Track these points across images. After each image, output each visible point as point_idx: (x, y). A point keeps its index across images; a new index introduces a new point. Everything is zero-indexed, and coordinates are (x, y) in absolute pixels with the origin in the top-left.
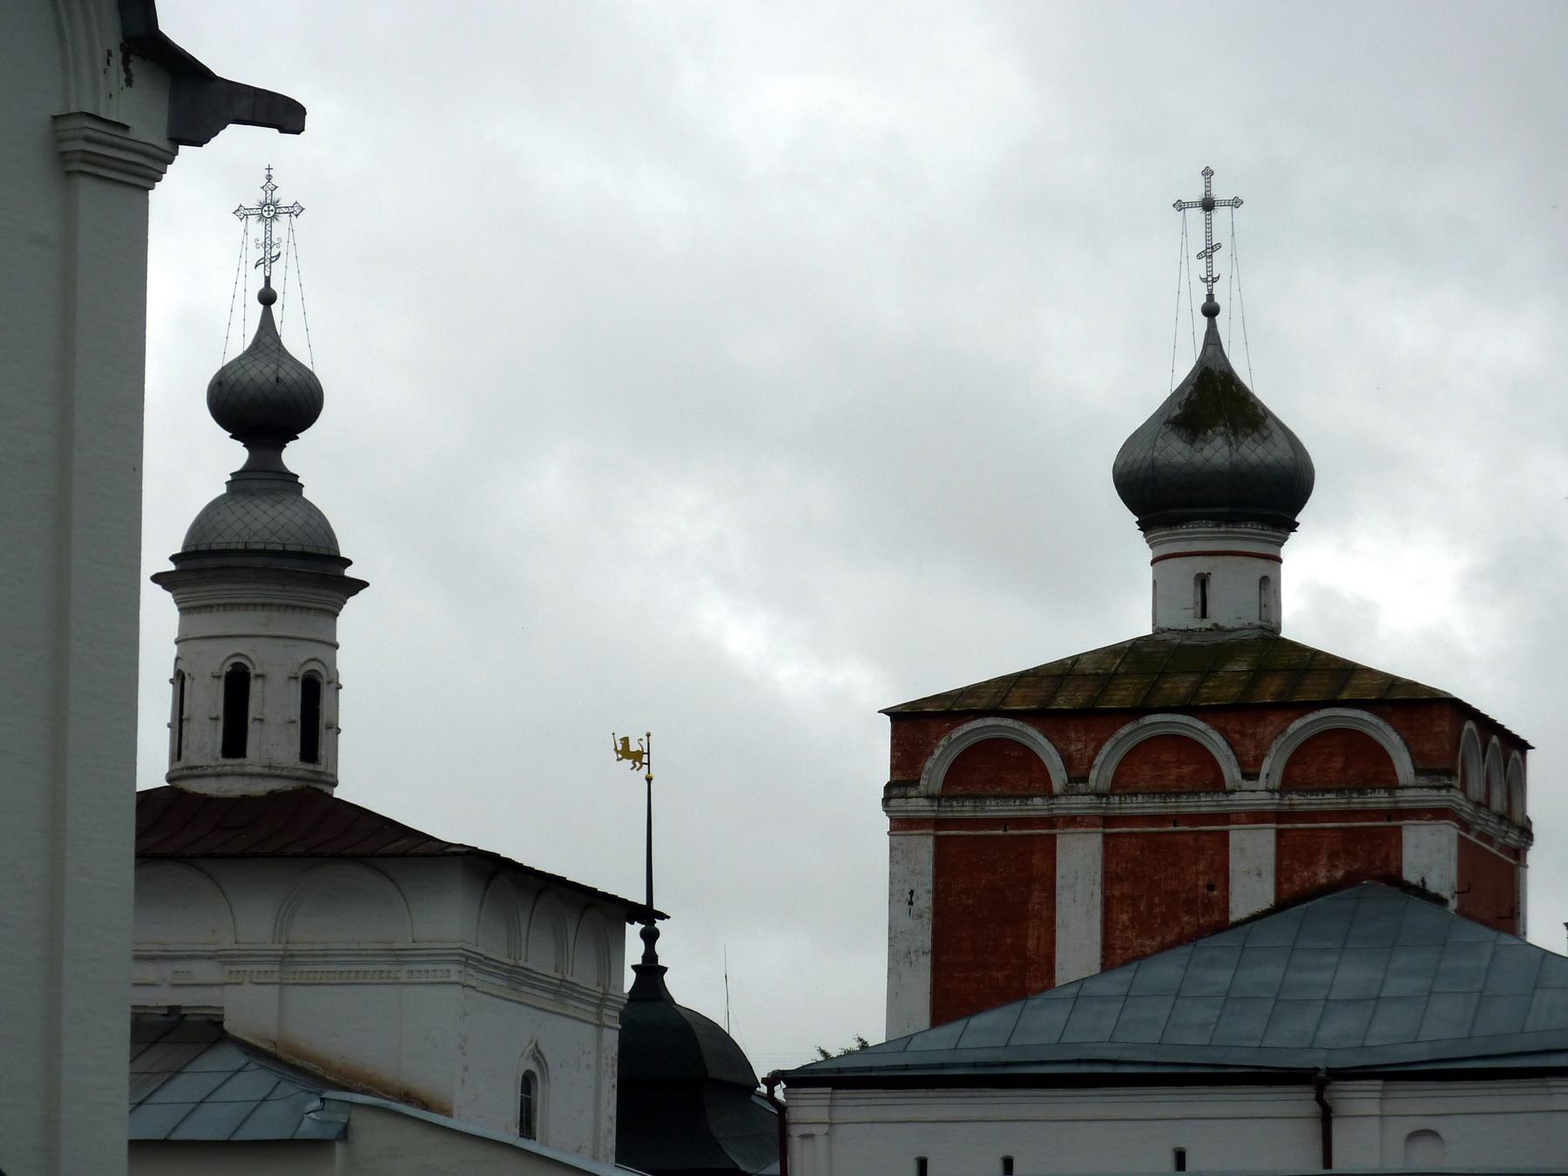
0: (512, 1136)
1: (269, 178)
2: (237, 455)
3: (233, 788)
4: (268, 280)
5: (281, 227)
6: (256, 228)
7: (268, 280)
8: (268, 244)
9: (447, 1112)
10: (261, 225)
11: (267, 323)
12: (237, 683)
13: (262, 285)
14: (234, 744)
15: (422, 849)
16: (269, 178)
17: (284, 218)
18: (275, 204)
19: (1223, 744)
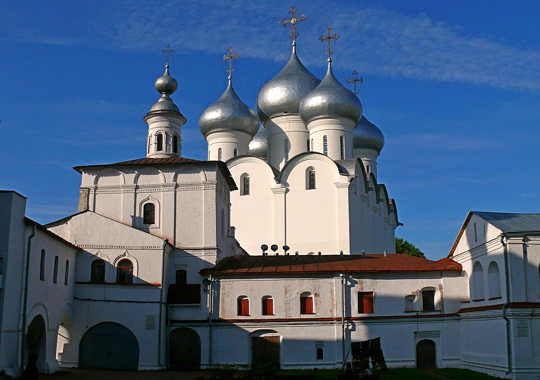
3: (159, 157)
14: (159, 148)
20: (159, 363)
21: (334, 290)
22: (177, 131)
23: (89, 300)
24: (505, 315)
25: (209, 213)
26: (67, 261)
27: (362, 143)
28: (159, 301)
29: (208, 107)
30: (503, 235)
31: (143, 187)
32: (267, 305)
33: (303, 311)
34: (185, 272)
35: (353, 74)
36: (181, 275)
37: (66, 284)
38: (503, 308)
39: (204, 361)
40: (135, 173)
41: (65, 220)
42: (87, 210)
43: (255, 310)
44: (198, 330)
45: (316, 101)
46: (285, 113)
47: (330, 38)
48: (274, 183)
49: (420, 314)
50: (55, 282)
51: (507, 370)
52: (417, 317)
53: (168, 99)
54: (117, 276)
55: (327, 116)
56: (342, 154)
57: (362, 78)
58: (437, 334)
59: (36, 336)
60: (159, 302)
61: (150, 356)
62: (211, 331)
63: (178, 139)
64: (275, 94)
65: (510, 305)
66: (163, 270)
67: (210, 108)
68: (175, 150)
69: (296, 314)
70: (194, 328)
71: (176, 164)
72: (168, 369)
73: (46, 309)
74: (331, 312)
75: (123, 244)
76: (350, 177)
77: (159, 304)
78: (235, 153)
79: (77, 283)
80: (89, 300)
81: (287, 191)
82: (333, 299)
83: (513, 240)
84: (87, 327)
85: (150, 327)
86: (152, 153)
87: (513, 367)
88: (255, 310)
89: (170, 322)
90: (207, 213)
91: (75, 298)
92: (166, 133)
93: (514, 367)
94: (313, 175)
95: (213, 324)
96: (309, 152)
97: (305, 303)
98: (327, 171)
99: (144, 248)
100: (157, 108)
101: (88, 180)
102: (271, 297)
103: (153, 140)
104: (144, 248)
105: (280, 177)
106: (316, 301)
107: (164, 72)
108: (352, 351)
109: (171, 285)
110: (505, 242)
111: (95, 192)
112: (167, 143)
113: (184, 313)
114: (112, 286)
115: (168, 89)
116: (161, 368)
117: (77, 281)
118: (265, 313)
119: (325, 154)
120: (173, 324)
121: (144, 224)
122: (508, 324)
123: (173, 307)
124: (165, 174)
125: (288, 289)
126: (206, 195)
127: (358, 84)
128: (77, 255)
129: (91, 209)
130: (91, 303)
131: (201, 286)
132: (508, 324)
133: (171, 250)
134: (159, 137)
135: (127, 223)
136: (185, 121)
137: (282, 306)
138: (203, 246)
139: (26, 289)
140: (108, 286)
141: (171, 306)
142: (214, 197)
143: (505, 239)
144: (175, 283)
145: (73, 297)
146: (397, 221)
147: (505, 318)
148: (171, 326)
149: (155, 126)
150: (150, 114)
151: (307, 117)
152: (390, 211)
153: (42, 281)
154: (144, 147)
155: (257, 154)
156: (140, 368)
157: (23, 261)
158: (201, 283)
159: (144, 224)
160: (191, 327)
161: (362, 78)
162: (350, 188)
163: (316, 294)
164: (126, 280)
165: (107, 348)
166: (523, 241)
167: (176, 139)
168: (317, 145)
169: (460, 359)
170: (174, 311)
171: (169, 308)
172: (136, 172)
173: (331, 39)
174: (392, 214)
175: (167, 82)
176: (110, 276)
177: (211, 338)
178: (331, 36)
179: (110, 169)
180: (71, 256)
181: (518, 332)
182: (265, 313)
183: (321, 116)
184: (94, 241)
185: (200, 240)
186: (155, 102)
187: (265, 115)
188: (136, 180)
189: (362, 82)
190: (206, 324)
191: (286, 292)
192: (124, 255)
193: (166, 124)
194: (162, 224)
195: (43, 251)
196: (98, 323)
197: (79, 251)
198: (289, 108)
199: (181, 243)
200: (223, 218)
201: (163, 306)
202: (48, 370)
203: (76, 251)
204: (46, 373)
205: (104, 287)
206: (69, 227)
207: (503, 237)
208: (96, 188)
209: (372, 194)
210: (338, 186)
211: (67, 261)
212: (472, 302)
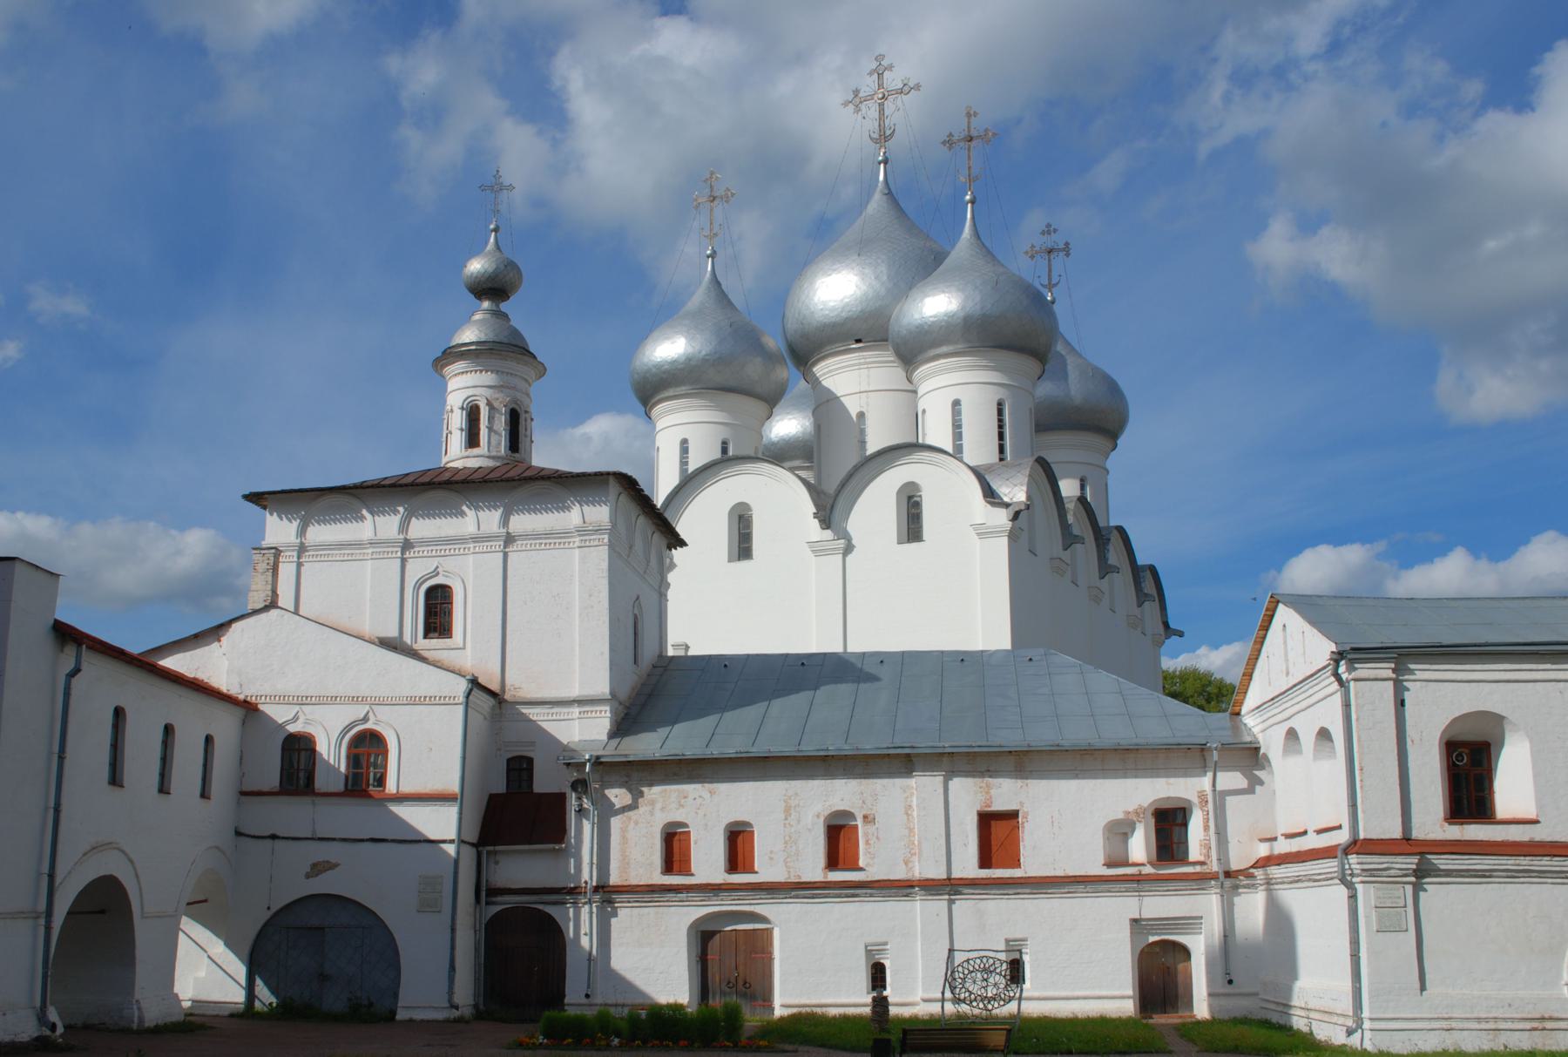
3: (473, 463)
14: (472, 440)
20: (450, 1000)
21: (914, 804)
22: (519, 395)
23: (274, 837)
24: (1344, 875)
26: (209, 740)
27: (1063, 420)
29: (651, 331)
30: (1338, 657)
32: (738, 843)
33: (833, 862)
34: (530, 761)
35: (1043, 233)
36: (520, 768)
37: (204, 795)
38: (1339, 854)
40: (396, 512)
41: (216, 632)
42: (272, 605)
43: (708, 862)
45: (937, 304)
46: (858, 341)
47: (971, 139)
48: (814, 530)
49: (1148, 870)
50: (163, 789)
51: (1350, 1023)
52: (1138, 879)
53: (499, 315)
55: (960, 347)
56: (1002, 449)
57: (1067, 244)
58: (1189, 923)
59: (101, 924)
61: (436, 972)
64: (836, 289)
65: (1358, 846)
66: (464, 758)
67: (656, 334)
68: (514, 442)
69: (813, 867)
71: (515, 481)
73: (131, 861)
74: (906, 864)
75: (364, 690)
76: (1011, 511)
78: (724, 450)
79: (244, 793)
80: (274, 837)
81: (849, 549)
82: (911, 830)
83: (1364, 670)
85: (427, 905)
86: (456, 455)
87: (1366, 1014)
88: (708, 862)
89: (485, 892)
91: (238, 833)
92: (489, 404)
94: (918, 505)
96: (914, 447)
97: (839, 838)
98: (951, 494)
99: (414, 701)
100: (469, 335)
101: (279, 529)
102: (686, 825)
103: (457, 420)
104: (414, 701)
105: (830, 508)
106: (866, 834)
107: (487, 243)
110: (1344, 677)
112: (490, 429)
113: (520, 869)
114: (333, 800)
115: (493, 289)
116: (456, 1014)
117: (246, 788)
118: (668, 868)
119: (957, 453)
121: (426, 637)
122: (1353, 897)
123: (496, 853)
124: (585, 508)
125: (793, 803)
127: (1058, 261)
129: (285, 599)
130: (279, 844)
132: (1353, 897)
133: (491, 703)
134: (473, 414)
136: (542, 370)
138: (575, 692)
139: (57, 810)
141: (488, 853)
142: (605, 565)
143: (1342, 669)
146: (1166, 625)
147: (1343, 881)
148: (487, 903)
149: (464, 385)
150: (451, 354)
151: (912, 351)
152: (1142, 597)
154: (435, 435)
155: (780, 455)
156: (401, 1015)
159: (426, 637)
160: (540, 907)
161: (1067, 244)
162: (1013, 536)
163: (865, 817)
165: (318, 956)
166: (1394, 671)
167: (515, 418)
168: (937, 432)
169: (1256, 994)
170: (497, 863)
172: (401, 509)
173: (973, 144)
174: (1151, 608)
175: (491, 270)
178: (974, 133)
180: (225, 726)
181: (1380, 920)
182: (1109, 865)
183: (944, 349)
184: (289, 684)
185: (568, 682)
186: (466, 320)
187: (807, 349)
188: (404, 527)
189: (1068, 255)
191: (787, 811)
192: (365, 719)
193: (488, 378)
194: (472, 644)
195: (119, 713)
197: (248, 709)
198: (863, 331)
199: (522, 683)
200: (1536, 653)
202: (141, 1019)
203: (239, 713)
204: (135, 1026)
205: (314, 804)
206: (223, 650)
207: (1337, 662)
208: (302, 549)
209: (1086, 552)
210: (983, 532)
211: (209, 740)
212: (1281, 839)
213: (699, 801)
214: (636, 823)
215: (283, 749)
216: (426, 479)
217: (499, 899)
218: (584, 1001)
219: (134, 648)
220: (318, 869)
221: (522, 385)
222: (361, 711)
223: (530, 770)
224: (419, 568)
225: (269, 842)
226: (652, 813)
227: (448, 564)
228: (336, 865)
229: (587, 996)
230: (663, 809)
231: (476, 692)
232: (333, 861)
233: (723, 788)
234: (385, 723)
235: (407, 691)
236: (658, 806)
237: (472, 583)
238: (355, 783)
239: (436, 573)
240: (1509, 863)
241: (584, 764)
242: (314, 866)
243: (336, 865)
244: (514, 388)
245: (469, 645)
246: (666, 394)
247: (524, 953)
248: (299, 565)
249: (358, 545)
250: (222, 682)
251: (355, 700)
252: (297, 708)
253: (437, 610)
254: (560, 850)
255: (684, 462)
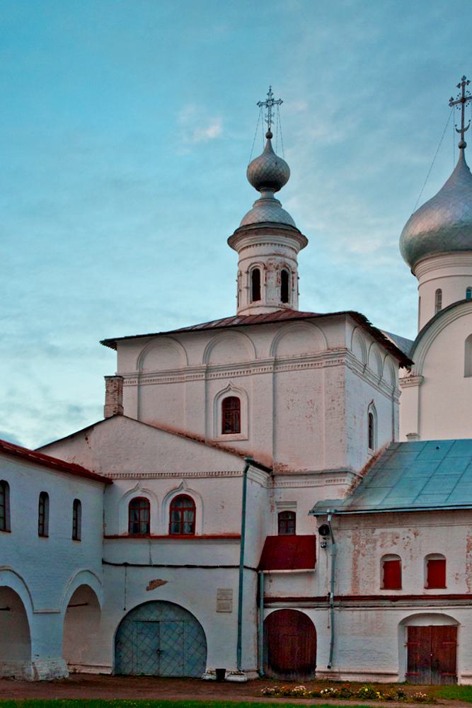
0: (214, 429)
1: (270, 90)
2: (258, 195)
3: (256, 312)
4: (269, 129)
5: (274, 109)
6: (265, 110)
7: (269, 129)
8: (270, 115)
9: (356, 506)
10: (265, 101)
11: (269, 144)
12: (255, 275)
13: (267, 131)
14: (256, 296)
15: (293, 316)
16: (270, 90)
17: (275, 105)
18: (273, 100)
19: (106, 673)
25: (334, 408)
28: (238, 564)
31: (218, 369)
32: (436, 571)
34: (294, 514)
39: (321, 665)
43: (414, 580)
44: (310, 613)
54: (170, 525)
60: (238, 567)
61: (231, 649)
62: (253, 569)
63: (291, 276)
68: (285, 297)
70: (305, 611)
72: (263, 678)
75: (179, 469)
77: (236, 572)
79: (106, 537)
80: (126, 565)
84: (125, 609)
85: (223, 609)
88: (414, 580)
89: (263, 600)
90: (330, 409)
91: (104, 562)
93: (143, 507)
95: (338, 603)
99: (212, 476)
100: (143, 638)
104: (212, 476)
108: (445, 627)
109: (269, 539)
111: (139, 382)
113: (285, 586)
117: (110, 532)
120: (269, 604)
121: (223, 433)
126: (328, 375)
128: (104, 493)
130: (129, 569)
131: (317, 537)
135: (199, 431)
136: (304, 242)
137: (460, 573)
140: (156, 541)
141: (265, 575)
144: (277, 535)
145: (101, 562)
148: (265, 607)
153: (8, 534)
157: (327, 565)
158: (317, 534)
159: (223, 433)
160: (300, 610)
164: (187, 529)
170: (271, 581)
171: (262, 577)
176: (160, 522)
177: (332, 627)
179: (163, 340)
190: (324, 604)
194: (254, 435)
196: (142, 602)
201: (250, 577)
205: (150, 543)
213: (407, 540)
214: (363, 555)
215: (94, 592)
216: (223, 324)
217: (273, 604)
218: (327, 670)
219: (31, 445)
220: (154, 584)
221: (290, 253)
222: (178, 482)
223: (294, 520)
224: (218, 386)
225: (123, 568)
226: (374, 548)
227: (238, 382)
228: (165, 582)
229: (329, 667)
230: (382, 546)
231: (251, 467)
232: (163, 580)
233: (424, 531)
234: (194, 488)
235: (205, 469)
236: (379, 543)
237: (254, 393)
238: (176, 530)
239: (228, 389)
240: (387, 603)
241: (326, 516)
242: (152, 582)
243: (165, 582)
244: (284, 256)
245: (252, 437)
246: (417, 262)
247: (287, 643)
248: (463, 110)
249: (179, 372)
250: (89, 465)
251: (174, 476)
252: (137, 482)
253: (231, 410)
254: (313, 572)
255: (438, 305)
